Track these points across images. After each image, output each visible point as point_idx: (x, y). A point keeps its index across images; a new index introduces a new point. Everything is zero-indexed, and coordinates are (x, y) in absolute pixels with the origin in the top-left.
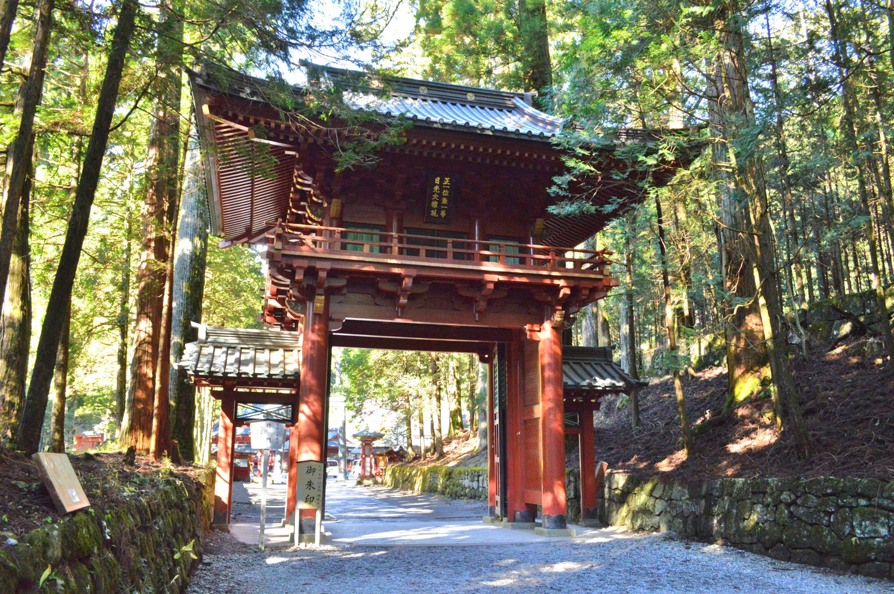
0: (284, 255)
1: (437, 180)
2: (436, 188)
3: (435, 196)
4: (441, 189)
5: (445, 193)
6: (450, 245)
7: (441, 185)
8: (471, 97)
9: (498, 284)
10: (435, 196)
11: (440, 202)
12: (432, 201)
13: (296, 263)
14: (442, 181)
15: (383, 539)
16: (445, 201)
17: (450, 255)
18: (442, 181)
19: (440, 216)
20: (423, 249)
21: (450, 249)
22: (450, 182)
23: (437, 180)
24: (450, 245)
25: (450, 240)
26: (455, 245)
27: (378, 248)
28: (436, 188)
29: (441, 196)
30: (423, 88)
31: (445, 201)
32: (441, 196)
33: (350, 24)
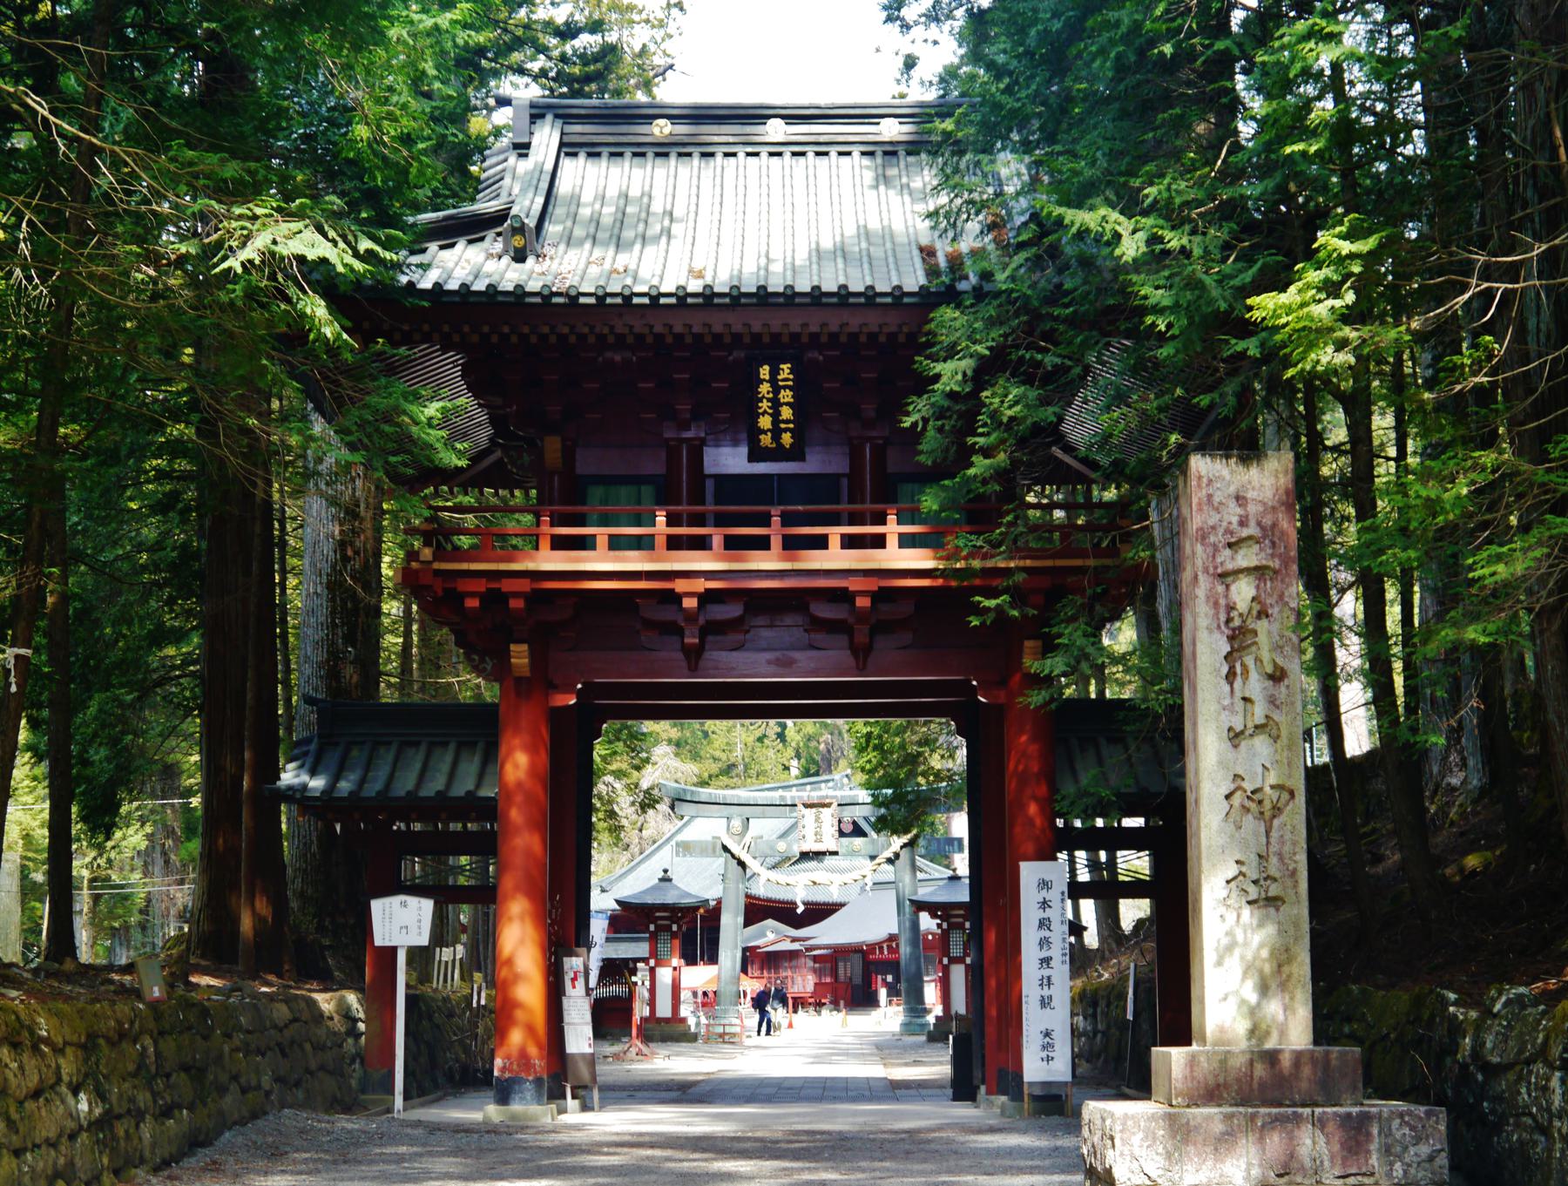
0: (438, 573)
1: (765, 372)
2: (765, 388)
3: (765, 405)
4: (776, 389)
5: (786, 396)
6: (776, 520)
7: (773, 380)
8: (776, 130)
9: (707, 597)
10: (765, 405)
11: (776, 415)
12: (758, 415)
13: (464, 586)
14: (774, 372)
15: (916, 1063)
16: (786, 413)
17: (776, 542)
18: (774, 372)
19: (780, 446)
20: (835, 533)
21: (775, 532)
22: (792, 371)
23: (765, 372)
24: (776, 520)
25: (775, 511)
26: (788, 520)
27: (896, 538)
28: (765, 388)
29: (776, 404)
30: (662, 122)
31: (786, 413)
32: (776, 404)
33: (229, 28)
